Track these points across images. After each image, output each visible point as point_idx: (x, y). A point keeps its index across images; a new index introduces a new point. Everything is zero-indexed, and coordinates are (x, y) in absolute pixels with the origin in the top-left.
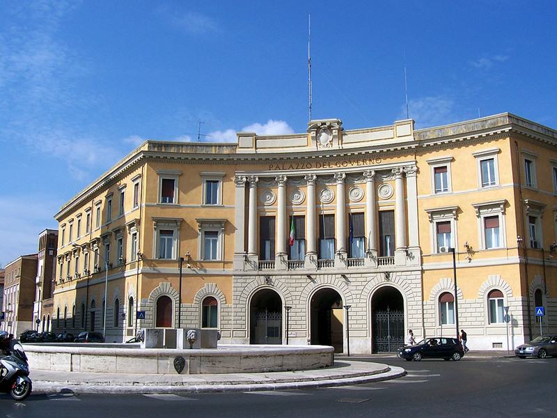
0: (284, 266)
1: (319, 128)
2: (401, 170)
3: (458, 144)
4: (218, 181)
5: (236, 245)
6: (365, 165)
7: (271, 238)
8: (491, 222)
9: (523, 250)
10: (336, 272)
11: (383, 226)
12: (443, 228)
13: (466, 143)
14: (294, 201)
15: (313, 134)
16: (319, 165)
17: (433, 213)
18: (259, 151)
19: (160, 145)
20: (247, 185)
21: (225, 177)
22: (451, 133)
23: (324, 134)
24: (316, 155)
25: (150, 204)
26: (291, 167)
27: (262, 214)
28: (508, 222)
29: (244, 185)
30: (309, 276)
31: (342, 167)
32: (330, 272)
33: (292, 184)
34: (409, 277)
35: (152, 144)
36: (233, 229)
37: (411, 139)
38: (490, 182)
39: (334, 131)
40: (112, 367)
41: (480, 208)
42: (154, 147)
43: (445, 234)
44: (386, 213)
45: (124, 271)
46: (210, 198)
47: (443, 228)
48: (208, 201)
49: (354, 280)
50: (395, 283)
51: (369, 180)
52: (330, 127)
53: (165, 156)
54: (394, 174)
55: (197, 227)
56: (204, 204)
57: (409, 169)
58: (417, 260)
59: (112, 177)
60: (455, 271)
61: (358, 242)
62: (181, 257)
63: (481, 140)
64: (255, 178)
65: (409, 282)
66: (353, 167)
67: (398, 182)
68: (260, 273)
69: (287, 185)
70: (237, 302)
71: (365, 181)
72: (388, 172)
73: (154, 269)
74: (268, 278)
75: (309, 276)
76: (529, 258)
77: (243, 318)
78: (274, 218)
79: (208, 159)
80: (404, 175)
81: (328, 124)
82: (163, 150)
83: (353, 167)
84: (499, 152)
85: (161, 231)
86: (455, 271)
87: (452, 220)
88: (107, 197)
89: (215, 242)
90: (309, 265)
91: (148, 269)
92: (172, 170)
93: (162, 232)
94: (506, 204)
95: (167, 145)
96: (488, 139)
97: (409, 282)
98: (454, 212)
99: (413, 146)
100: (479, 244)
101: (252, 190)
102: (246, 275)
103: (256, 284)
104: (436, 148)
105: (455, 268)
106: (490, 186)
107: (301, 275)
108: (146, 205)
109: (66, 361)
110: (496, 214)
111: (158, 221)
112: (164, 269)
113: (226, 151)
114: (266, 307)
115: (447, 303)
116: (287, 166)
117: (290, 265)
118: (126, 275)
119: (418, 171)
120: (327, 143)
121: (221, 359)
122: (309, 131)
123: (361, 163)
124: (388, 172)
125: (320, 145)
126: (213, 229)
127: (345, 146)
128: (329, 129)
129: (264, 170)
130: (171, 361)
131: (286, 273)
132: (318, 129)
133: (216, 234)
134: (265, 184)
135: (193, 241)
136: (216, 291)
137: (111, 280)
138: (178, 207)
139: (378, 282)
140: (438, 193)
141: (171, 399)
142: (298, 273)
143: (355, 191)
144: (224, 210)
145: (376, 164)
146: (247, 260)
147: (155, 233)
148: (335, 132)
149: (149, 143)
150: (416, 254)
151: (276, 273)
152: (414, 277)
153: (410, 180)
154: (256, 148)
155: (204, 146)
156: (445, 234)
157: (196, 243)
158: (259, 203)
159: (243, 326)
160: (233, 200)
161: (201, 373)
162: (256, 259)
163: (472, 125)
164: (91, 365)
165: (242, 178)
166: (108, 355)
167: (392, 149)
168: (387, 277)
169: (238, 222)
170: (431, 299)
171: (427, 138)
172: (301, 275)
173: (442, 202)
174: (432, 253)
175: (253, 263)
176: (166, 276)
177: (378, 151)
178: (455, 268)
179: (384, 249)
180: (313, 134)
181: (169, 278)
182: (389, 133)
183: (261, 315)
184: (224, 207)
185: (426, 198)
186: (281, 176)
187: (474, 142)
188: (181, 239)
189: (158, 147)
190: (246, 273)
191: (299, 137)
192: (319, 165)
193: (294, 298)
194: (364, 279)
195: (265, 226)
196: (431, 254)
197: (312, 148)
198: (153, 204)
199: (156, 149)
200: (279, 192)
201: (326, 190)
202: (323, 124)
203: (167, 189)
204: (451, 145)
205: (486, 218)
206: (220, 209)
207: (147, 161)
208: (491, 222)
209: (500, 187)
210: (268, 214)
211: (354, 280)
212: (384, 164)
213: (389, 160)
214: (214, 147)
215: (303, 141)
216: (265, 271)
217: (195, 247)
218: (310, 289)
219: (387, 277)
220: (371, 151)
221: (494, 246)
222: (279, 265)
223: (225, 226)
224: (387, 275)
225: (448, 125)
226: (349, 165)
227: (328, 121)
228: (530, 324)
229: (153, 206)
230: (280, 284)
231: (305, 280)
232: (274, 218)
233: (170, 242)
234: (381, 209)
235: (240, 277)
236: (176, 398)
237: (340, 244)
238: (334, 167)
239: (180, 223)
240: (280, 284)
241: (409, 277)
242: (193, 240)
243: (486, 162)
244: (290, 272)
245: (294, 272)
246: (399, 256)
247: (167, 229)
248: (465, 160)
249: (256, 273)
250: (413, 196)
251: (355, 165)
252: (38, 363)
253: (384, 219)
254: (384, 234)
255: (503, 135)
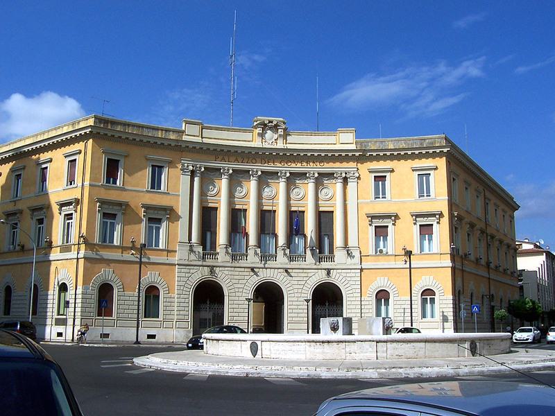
0: (228, 258)
1: (265, 125)
2: (344, 175)
3: (399, 157)
4: (163, 167)
5: (179, 234)
6: (315, 166)
7: (212, 230)
8: (426, 230)
9: (454, 255)
10: (278, 266)
11: (322, 225)
12: (381, 232)
13: (406, 157)
14: (237, 194)
15: (259, 130)
16: (263, 161)
17: (373, 217)
18: (205, 141)
19: (106, 122)
20: (193, 174)
21: (171, 164)
22: (391, 146)
23: (269, 131)
24: (271, 152)
25: (94, 183)
26: (236, 160)
27: (205, 204)
28: (441, 231)
29: (189, 174)
30: (252, 269)
31: (286, 165)
32: (275, 266)
33: (237, 178)
34: (348, 275)
35: (98, 120)
36: (178, 218)
37: (353, 147)
38: (425, 195)
39: (279, 130)
40: (421, 353)
41: (417, 216)
42: (100, 122)
43: (427, 236)
44: (325, 214)
45: (48, 254)
46: (155, 183)
47: (381, 232)
48: (153, 187)
49: (296, 275)
50: (336, 279)
51: (339, 181)
52: (276, 126)
53: (99, 131)
54: (337, 178)
55: (142, 212)
56: (149, 189)
57: (351, 175)
58: (357, 259)
59: (26, 149)
60: (410, 271)
61: (297, 239)
62: (403, 253)
63: (420, 156)
64: (200, 167)
65: (349, 279)
66: (297, 167)
67: (339, 186)
68: (204, 263)
69: (231, 178)
70: (181, 292)
71: (306, 182)
72: (330, 175)
73: (97, 254)
74: (212, 268)
75: (252, 269)
76: (456, 263)
77: (186, 309)
78: (216, 209)
79: (141, 141)
80: (345, 180)
81: (275, 123)
82: (109, 127)
83: (297, 167)
84: (436, 169)
85: (104, 213)
86: (410, 271)
87: (435, 224)
88: (12, 170)
89: (158, 229)
90: (253, 259)
91: (91, 254)
92: (119, 149)
93: (105, 215)
94: (441, 215)
95: (114, 123)
96: (427, 156)
97: (349, 279)
98: (393, 218)
99: (357, 154)
100: (416, 250)
101: (197, 180)
102: (192, 266)
103: (200, 275)
104: (378, 158)
105: (410, 268)
106: (425, 197)
107: (245, 268)
108: (90, 185)
109: (370, 349)
110: (431, 223)
111: (103, 202)
112: (107, 254)
113: (172, 136)
114: (208, 297)
115: (383, 300)
116: (232, 159)
117: (234, 258)
118: (51, 258)
119: (359, 178)
120: (271, 141)
121: (493, 342)
122: (256, 127)
123: (305, 164)
124: (330, 175)
125: (265, 142)
126: (158, 215)
127: (290, 146)
128: (275, 128)
129: (210, 162)
130: (467, 345)
131: (229, 265)
132: (264, 126)
133: (159, 221)
134: (209, 176)
135: (136, 227)
136: (388, 284)
137: (39, 262)
138: (122, 189)
139: (318, 277)
140: (377, 200)
141: (287, 383)
142: (242, 265)
143: (296, 190)
144: (169, 197)
145: (319, 166)
146: (191, 250)
147: (98, 216)
148: (281, 132)
149: (96, 117)
150: (356, 253)
151: (221, 264)
152: (354, 275)
153: (352, 185)
154: (202, 138)
155: (150, 128)
156: (427, 236)
157: (140, 229)
158: (203, 194)
159: (186, 317)
160: (178, 187)
161: (480, 355)
162: (200, 249)
163: (411, 141)
164: (400, 352)
165: (188, 166)
166: (403, 342)
167: (337, 154)
168: (328, 274)
169: (182, 210)
170: (368, 295)
171: (368, 148)
172: (245, 268)
173: (381, 207)
174: (370, 253)
175: (197, 253)
176: (109, 262)
177: (323, 154)
178: (410, 268)
179: (322, 247)
180: (259, 130)
181: (112, 265)
182: (332, 139)
183: (202, 306)
184: (169, 193)
185: (367, 203)
186: (226, 168)
187: (413, 157)
188: (124, 224)
189: (104, 123)
190: (192, 263)
191: (245, 131)
192: (263, 161)
193: (237, 290)
194: (306, 275)
195: (208, 215)
196: (369, 254)
197: (257, 143)
198: (97, 184)
199: (102, 126)
200: (223, 183)
201: (268, 186)
202: (270, 122)
203: (112, 169)
204: (392, 158)
205: (420, 225)
206: (165, 196)
207: (93, 138)
208: (426, 230)
209: (435, 200)
210: (210, 205)
211: (296, 275)
212: (328, 167)
213: (331, 165)
214: (160, 131)
215: (248, 136)
216: (209, 262)
217: (140, 232)
218: (253, 281)
219: (328, 274)
220: (316, 154)
221: (426, 250)
222: (222, 256)
223: (169, 213)
224: (329, 271)
225: (389, 139)
226: (293, 165)
227: (275, 120)
228: (456, 320)
229: (99, 186)
230: (224, 275)
231: (248, 273)
232: (216, 209)
233: (113, 226)
234: (321, 209)
235: (185, 267)
236: (291, 381)
237: (282, 240)
238: (279, 165)
239: (123, 206)
240: (224, 275)
241: (348, 275)
242: (137, 225)
243: (424, 176)
244: (233, 265)
245: (238, 265)
246: (340, 255)
247: (111, 212)
248: (403, 174)
249: (200, 263)
250: (353, 201)
251: (299, 165)
252: (323, 353)
253: (324, 219)
254: (323, 233)
255: (441, 155)
